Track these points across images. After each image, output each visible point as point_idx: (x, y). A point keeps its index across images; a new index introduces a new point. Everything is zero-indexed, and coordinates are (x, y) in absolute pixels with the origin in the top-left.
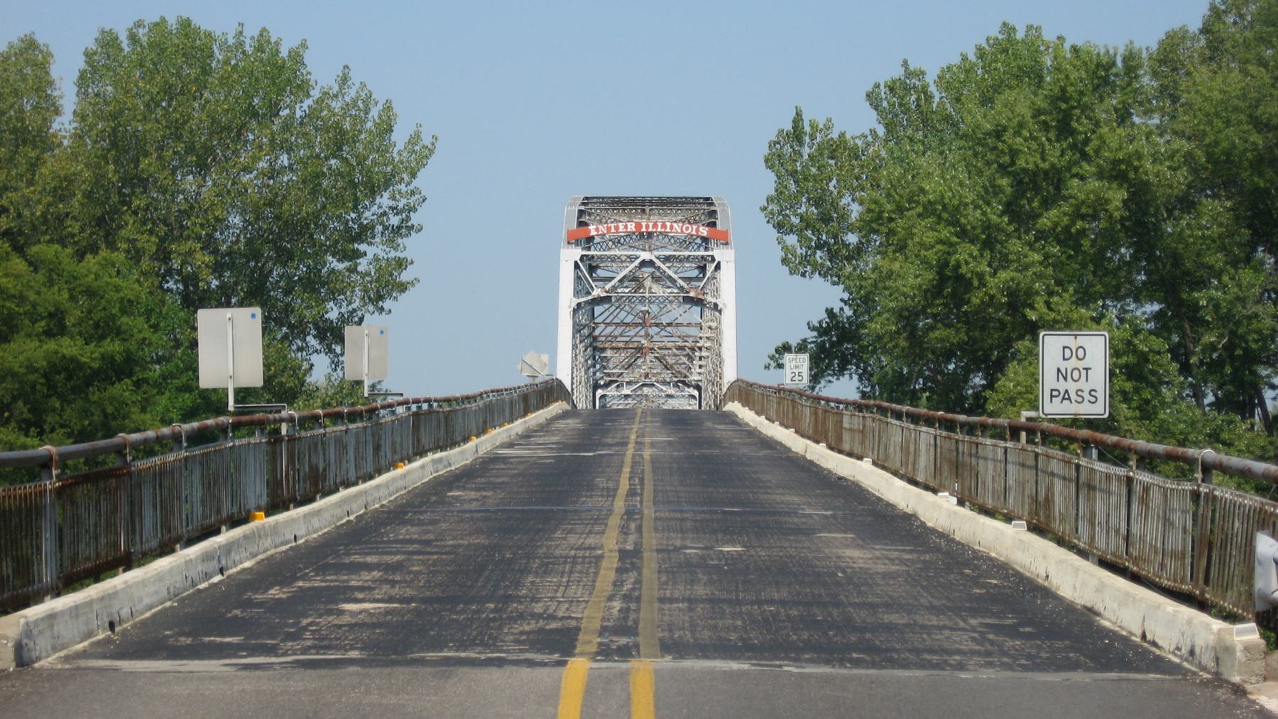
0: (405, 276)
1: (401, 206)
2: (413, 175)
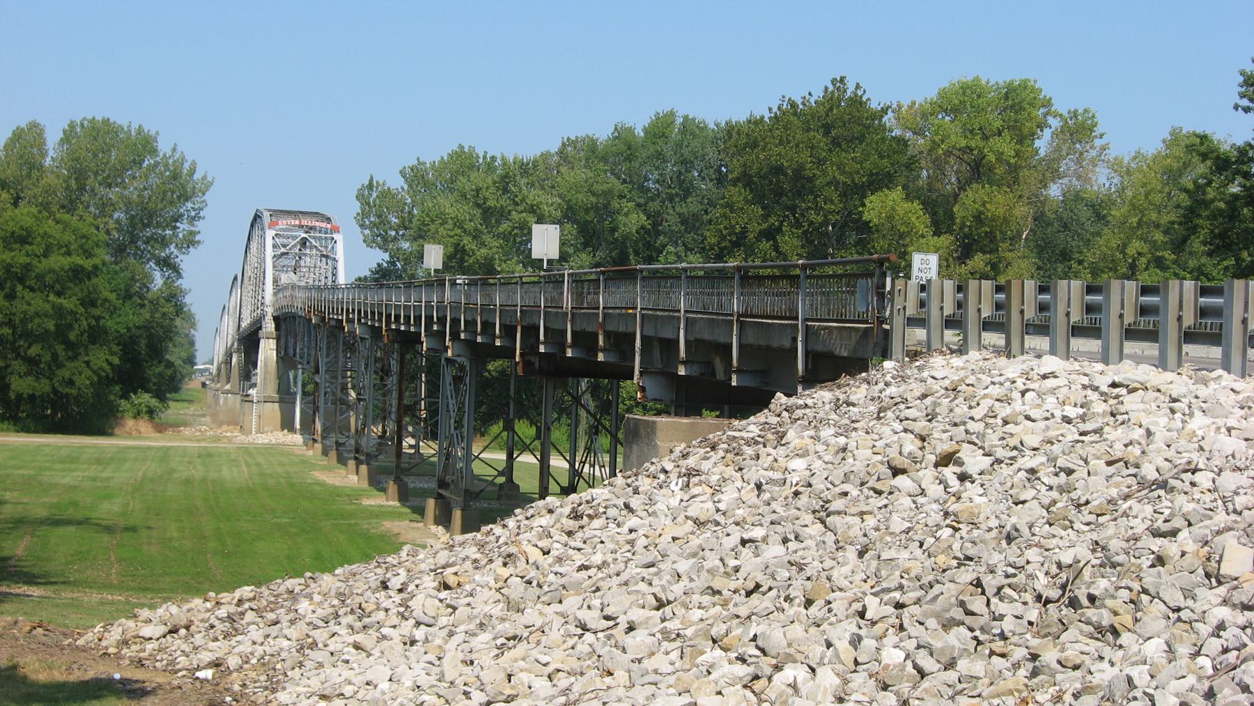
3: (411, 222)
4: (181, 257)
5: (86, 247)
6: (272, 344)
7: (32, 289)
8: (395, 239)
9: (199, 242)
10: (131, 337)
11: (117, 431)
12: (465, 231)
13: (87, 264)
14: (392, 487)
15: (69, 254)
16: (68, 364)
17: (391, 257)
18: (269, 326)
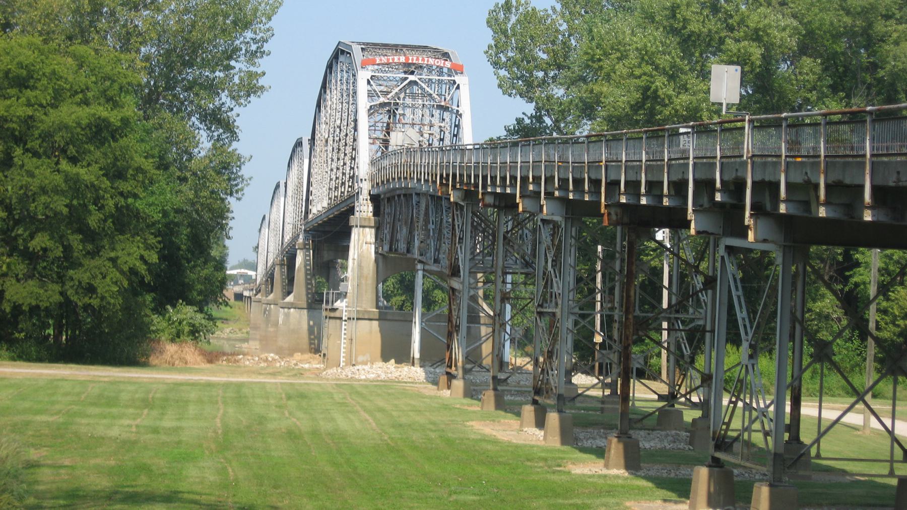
0: (262, 82)
1: (258, 38)
2: (270, 19)
3: (566, 57)
4: (237, 109)
5: (110, 93)
6: (369, 235)
7: (36, 154)
8: (543, 83)
9: (262, 88)
10: (167, 225)
11: (153, 360)
12: (657, 68)
13: (114, 117)
14: (615, 448)
15: (86, 102)
16: (86, 262)
17: (538, 109)
18: (364, 209)
